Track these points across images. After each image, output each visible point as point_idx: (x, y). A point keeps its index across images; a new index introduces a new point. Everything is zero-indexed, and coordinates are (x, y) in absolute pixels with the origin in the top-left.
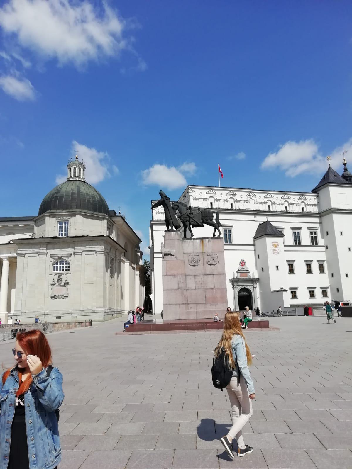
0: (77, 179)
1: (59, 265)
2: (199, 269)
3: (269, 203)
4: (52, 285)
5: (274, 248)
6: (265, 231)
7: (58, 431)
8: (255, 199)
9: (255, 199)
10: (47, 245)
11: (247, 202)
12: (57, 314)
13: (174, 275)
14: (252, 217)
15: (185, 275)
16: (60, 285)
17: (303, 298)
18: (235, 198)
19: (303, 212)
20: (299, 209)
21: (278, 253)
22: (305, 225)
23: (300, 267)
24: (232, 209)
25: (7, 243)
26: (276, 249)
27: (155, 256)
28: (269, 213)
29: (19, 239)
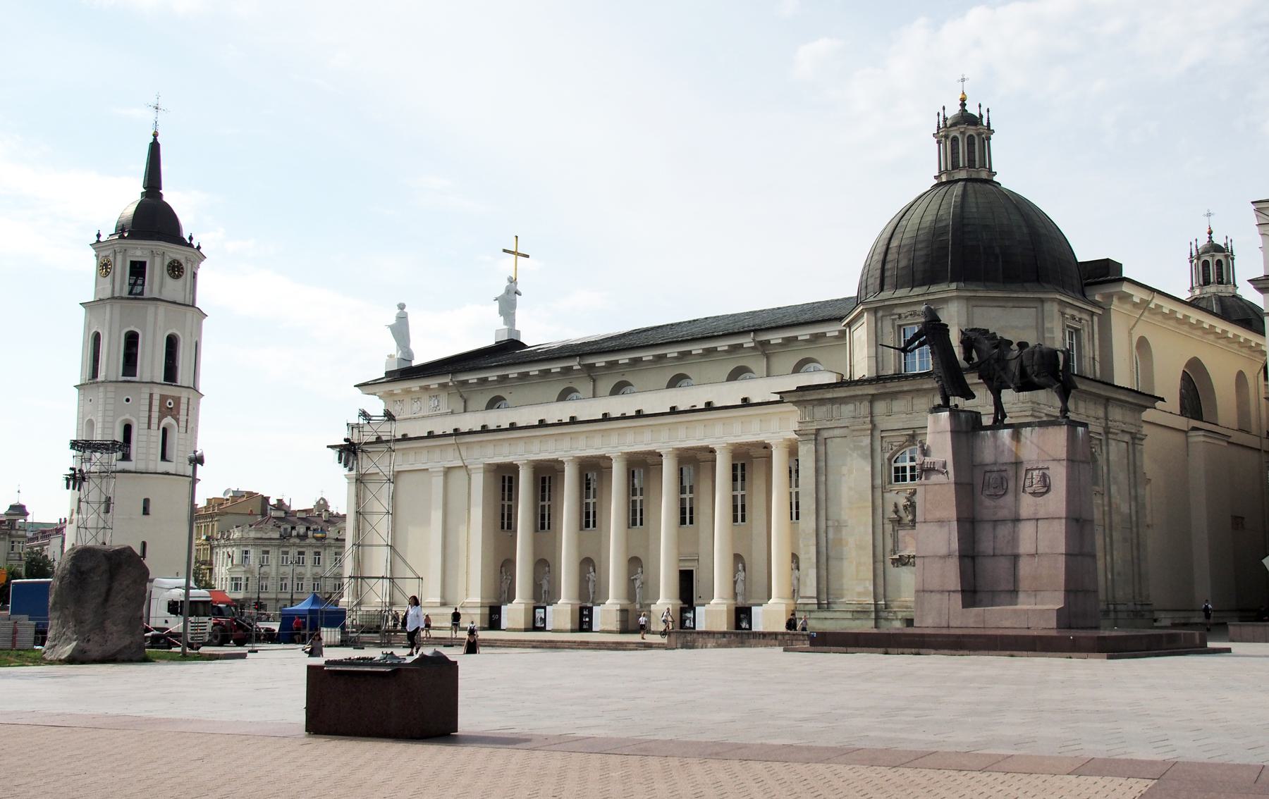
10: (871, 402)
29: (800, 389)
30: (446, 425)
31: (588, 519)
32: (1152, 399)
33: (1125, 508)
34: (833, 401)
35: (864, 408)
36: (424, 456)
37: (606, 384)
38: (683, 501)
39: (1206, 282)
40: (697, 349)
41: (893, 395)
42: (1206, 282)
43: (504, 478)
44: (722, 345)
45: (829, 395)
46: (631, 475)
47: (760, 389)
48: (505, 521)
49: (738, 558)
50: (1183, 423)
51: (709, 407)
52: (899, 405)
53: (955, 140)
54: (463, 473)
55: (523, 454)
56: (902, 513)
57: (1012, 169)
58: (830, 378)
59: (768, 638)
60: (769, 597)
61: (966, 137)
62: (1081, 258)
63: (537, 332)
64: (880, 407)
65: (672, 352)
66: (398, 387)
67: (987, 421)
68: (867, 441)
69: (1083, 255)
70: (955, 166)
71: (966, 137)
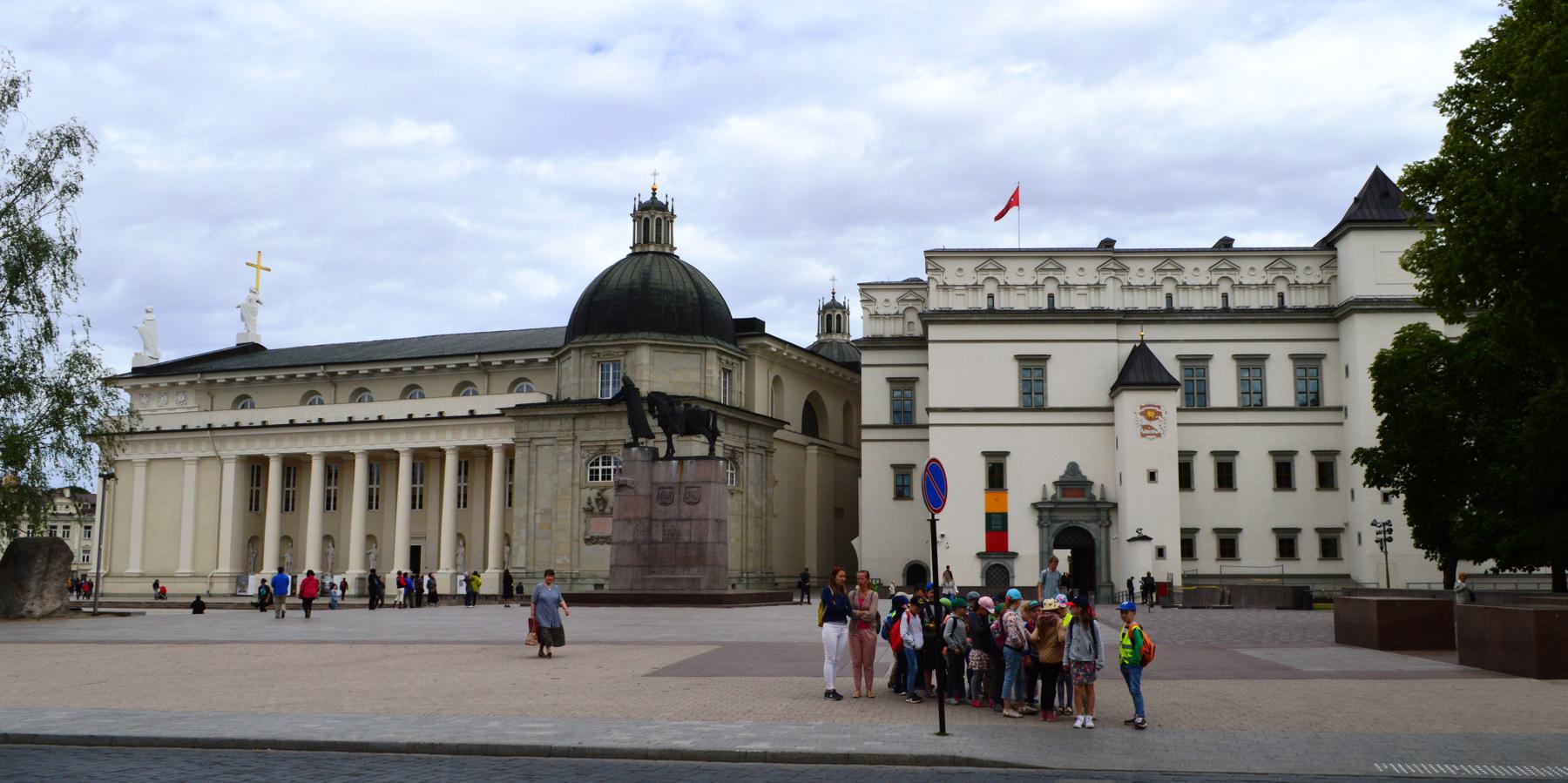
0: (652, 248)
1: (600, 467)
2: (672, 511)
3: (991, 287)
4: (586, 510)
5: (1146, 422)
6: (1139, 372)
7: (983, 711)
8: (1125, 279)
9: (1125, 279)
11: (1098, 287)
12: (596, 577)
13: (629, 520)
14: (1109, 331)
15: (651, 519)
16: (602, 513)
17: (1257, 556)
18: (1001, 278)
19: (1226, 309)
20: (1268, 300)
21: (1159, 435)
22: (1280, 351)
23: (1254, 472)
24: (1226, 309)
25: (466, 413)
26: (1154, 424)
27: (864, 436)
28: (1169, 315)
29: (518, 407)
30: (201, 420)
31: (289, 503)
32: (781, 424)
33: (758, 503)
34: (544, 417)
35: (568, 424)
36: (178, 447)
37: (346, 391)
38: (371, 490)
39: (829, 331)
40: (429, 365)
41: (591, 415)
42: (829, 331)
43: (255, 468)
44: (451, 364)
45: (541, 413)
46: (370, 467)
47: (486, 404)
48: (254, 502)
49: (460, 536)
50: (802, 439)
51: (441, 416)
52: (594, 423)
53: (647, 221)
54: (215, 463)
55: (273, 449)
56: (594, 504)
57: (691, 244)
58: (543, 399)
59: (489, 598)
60: (485, 567)
61: (653, 217)
62: (735, 315)
63: (273, 338)
64: (581, 423)
65: (407, 367)
66: (145, 383)
67: (662, 454)
68: (569, 449)
69: (736, 314)
70: (646, 241)
71: (653, 217)
